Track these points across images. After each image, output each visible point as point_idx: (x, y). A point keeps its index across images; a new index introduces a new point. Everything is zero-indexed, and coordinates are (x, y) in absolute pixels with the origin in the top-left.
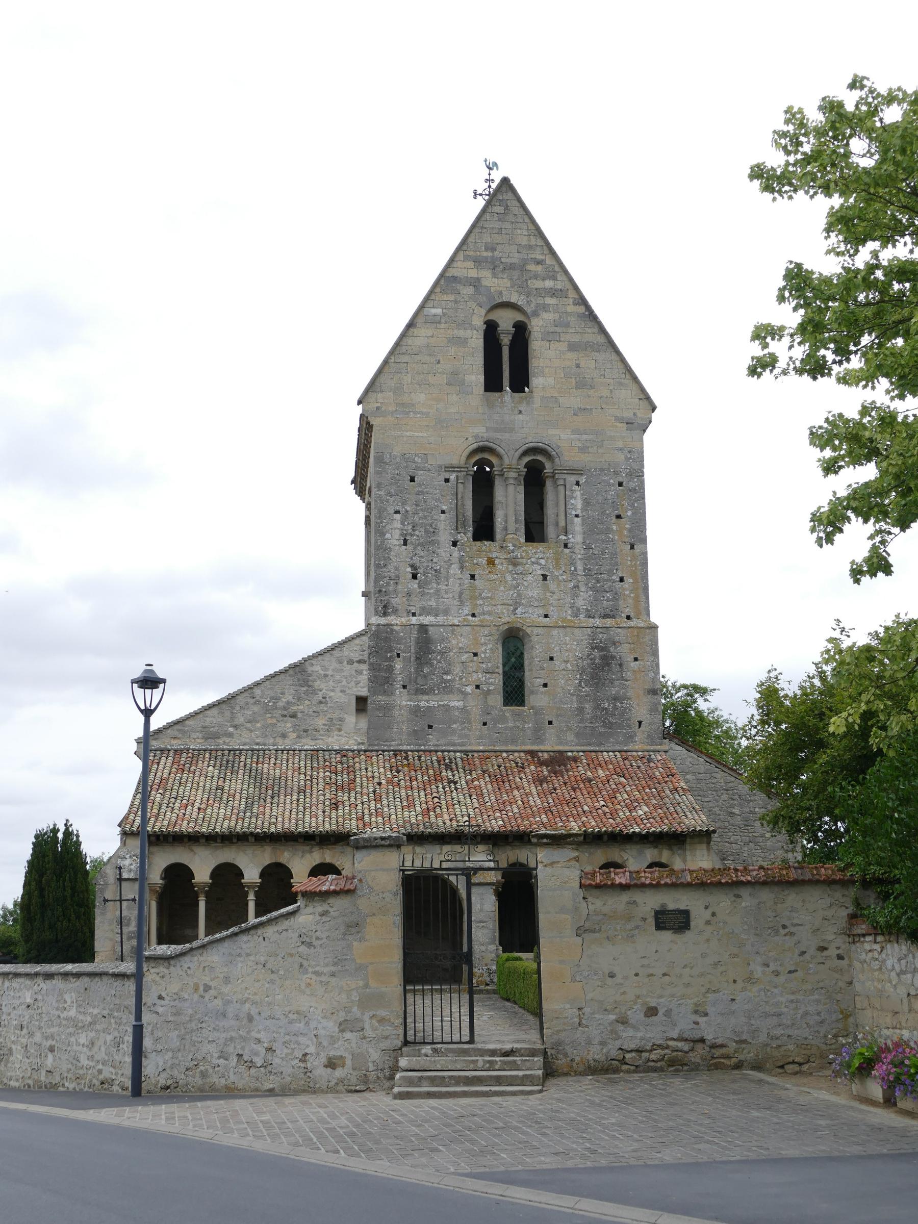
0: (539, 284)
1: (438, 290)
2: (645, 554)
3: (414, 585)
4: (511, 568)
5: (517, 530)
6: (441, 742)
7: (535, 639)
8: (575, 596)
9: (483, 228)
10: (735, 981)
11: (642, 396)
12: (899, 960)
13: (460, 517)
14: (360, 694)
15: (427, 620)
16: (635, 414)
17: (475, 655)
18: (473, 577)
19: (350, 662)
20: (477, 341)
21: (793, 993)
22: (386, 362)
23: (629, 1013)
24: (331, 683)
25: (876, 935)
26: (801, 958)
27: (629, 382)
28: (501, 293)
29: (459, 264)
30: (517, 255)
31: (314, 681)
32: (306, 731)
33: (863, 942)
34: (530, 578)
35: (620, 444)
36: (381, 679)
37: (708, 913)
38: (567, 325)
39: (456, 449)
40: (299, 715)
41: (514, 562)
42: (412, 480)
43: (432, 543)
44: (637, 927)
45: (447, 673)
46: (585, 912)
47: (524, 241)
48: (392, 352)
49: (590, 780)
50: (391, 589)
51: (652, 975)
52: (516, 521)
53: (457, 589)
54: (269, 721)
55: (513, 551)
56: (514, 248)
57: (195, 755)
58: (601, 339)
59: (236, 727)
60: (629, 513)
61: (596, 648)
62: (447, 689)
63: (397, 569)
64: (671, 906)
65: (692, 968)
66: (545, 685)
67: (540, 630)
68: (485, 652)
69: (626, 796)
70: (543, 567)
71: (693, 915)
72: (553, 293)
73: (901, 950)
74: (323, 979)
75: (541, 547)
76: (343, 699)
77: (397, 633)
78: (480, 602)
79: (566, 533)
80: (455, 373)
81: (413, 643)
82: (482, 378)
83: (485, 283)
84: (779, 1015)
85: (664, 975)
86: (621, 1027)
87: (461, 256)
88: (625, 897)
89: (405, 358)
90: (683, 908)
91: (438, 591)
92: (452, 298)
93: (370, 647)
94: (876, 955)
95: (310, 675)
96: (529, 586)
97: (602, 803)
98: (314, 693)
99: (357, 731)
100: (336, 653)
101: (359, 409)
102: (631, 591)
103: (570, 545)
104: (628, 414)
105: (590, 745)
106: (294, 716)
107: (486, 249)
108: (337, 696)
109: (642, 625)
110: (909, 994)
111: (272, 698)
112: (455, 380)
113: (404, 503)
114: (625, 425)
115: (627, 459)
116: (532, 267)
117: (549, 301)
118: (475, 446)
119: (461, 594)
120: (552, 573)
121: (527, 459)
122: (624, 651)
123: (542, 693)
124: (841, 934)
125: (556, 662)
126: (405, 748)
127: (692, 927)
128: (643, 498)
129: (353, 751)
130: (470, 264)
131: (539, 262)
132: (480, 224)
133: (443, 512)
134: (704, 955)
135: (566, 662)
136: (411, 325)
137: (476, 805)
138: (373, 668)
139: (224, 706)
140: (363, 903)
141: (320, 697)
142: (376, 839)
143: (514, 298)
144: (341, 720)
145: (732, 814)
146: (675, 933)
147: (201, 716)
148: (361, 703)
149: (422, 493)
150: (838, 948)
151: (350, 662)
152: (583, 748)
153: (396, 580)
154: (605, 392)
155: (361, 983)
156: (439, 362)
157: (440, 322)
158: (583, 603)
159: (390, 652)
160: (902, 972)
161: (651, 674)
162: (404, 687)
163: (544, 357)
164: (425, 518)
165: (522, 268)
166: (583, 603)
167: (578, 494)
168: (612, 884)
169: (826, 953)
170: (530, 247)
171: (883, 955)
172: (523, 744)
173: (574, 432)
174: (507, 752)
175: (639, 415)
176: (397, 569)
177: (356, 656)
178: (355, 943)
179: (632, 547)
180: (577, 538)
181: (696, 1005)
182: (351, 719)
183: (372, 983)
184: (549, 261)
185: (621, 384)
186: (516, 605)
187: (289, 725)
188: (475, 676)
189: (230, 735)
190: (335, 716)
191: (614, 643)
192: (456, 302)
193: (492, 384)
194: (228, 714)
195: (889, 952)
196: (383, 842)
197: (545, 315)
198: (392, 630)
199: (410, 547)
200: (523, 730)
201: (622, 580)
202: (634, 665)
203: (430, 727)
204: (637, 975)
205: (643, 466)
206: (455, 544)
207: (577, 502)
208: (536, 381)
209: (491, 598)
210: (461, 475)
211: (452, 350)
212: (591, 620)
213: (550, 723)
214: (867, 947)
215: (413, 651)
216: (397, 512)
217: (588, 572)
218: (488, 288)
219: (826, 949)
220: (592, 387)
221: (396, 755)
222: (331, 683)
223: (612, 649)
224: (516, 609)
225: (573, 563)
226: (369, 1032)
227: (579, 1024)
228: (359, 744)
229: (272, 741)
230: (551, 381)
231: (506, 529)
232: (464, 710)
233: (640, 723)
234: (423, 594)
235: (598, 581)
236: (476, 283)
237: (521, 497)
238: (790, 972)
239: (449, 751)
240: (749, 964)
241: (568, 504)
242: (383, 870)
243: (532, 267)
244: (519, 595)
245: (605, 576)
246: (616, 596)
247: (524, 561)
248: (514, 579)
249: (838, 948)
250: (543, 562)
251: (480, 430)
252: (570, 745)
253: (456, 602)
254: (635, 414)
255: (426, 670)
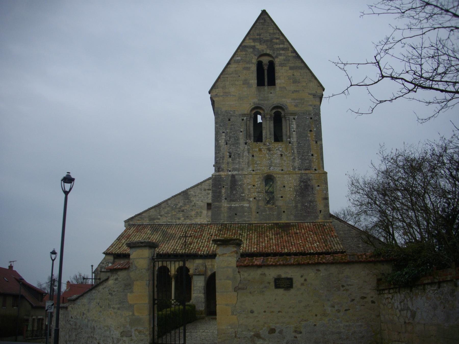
0: (277, 46)
1: (239, 51)
2: (321, 145)
3: (230, 160)
4: (268, 152)
5: (270, 138)
6: (240, 220)
7: (277, 179)
8: (294, 162)
9: (256, 28)
10: (316, 315)
11: (319, 85)
12: (400, 303)
13: (248, 133)
14: (208, 202)
15: (235, 173)
16: (316, 92)
17: (254, 186)
18: (253, 156)
19: (205, 190)
20: (254, 68)
21: (347, 322)
22: (219, 77)
23: (260, 331)
24: (197, 198)
25: (390, 289)
26: (352, 303)
27: (313, 80)
28: (263, 50)
29: (247, 41)
30: (269, 37)
31: (191, 197)
32: (187, 217)
33: (384, 294)
34: (275, 155)
35: (311, 103)
36: (217, 196)
37: (302, 280)
38: (289, 60)
39: (246, 108)
40: (185, 211)
41: (269, 150)
42: (229, 120)
43: (237, 143)
44: (265, 287)
45: (242, 193)
46: (239, 279)
47: (271, 31)
48: (222, 74)
49: (297, 233)
50: (221, 161)
51: (273, 312)
52: (270, 134)
53: (247, 161)
54: (174, 213)
55: (269, 145)
56: (268, 34)
57: (145, 226)
58: (303, 65)
59: (161, 216)
60: (315, 129)
61: (302, 182)
62: (243, 199)
63: (223, 154)
64: (283, 276)
65: (293, 308)
66: (282, 197)
67: (279, 176)
68: (258, 185)
69: (311, 239)
70: (281, 151)
71: (294, 280)
72: (283, 49)
73: (401, 297)
74: (115, 311)
75: (280, 144)
76: (202, 204)
77: (223, 178)
78: (256, 165)
79: (290, 138)
80: (246, 80)
81: (229, 182)
82: (256, 81)
83: (257, 47)
84: (339, 333)
85: (279, 312)
86: (256, 339)
87: (248, 38)
88: (260, 271)
89: (227, 76)
90: (289, 277)
91: (239, 162)
92: (244, 53)
93: (212, 184)
94: (390, 300)
95: (189, 195)
96: (277, 159)
97: (300, 242)
98: (191, 202)
99: (207, 216)
100: (199, 187)
101: (209, 96)
102: (316, 159)
103: (291, 142)
104: (314, 92)
105: (300, 220)
106: (183, 211)
107: (257, 35)
108: (200, 203)
109: (321, 172)
110: (405, 322)
111: (175, 204)
112: (246, 83)
113: (226, 129)
114: (312, 96)
115: (313, 109)
116: (275, 41)
117: (281, 52)
118: (253, 106)
119: (248, 163)
120: (284, 153)
121: (274, 111)
122: (314, 183)
123: (280, 200)
124: (374, 289)
125: (286, 188)
126: (226, 223)
127: (294, 287)
128: (320, 123)
129: (205, 224)
130: (251, 41)
131: (277, 39)
132: (255, 26)
133: (241, 132)
134: (300, 302)
135: (290, 188)
136: (229, 64)
137: (248, 243)
138: (214, 192)
139: (157, 208)
140: (132, 274)
141: (193, 204)
142: (138, 243)
143: (268, 52)
144: (201, 212)
145: (359, 247)
146: (285, 290)
147: (148, 212)
148: (209, 205)
149: (233, 125)
150: (372, 297)
151: (205, 190)
152: (297, 222)
153: (223, 158)
154: (304, 84)
155: (131, 313)
156: (239, 76)
157: (240, 62)
158: (297, 164)
159: (221, 186)
160: (402, 310)
161: (325, 192)
162: (226, 199)
163: (282, 75)
164: (234, 134)
165: (271, 41)
166: (297, 164)
167: (294, 123)
168: (252, 265)
169: (365, 300)
170: (274, 34)
171: (393, 300)
172: (273, 220)
173: (292, 99)
174: (266, 223)
175: (318, 92)
176: (223, 154)
177: (207, 187)
178: (129, 294)
179: (316, 142)
180: (294, 139)
181: (296, 328)
182: (205, 212)
183: (136, 314)
184: (281, 38)
185: (310, 81)
186: (270, 166)
187: (181, 215)
188: (254, 194)
189: (159, 219)
190: (199, 211)
191: (309, 180)
192: (246, 54)
193: (260, 83)
194: (158, 211)
195: (396, 298)
196: (141, 245)
197: (280, 57)
198: (221, 177)
199: (228, 146)
200: (273, 215)
201: (312, 155)
202: (317, 188)
203: (236, 214)
204: (265, 312)
205: (320, 111)
206: (246, 143)
207: (294, 126)
208: (277, 81)
209: (260, 164)
210: (248, 117)
211: (245, 72)
212: (300, 171)
213: (284, 212)
214: (386, 296)
215: (229, 184)
216: (223, 132)
217: (299, 152)
218: (258, 49)
219: (365, 298)
220: (299, 82)
221: (222, 225)
222: (197, 198)
223: (309, 182)
224: (270, 168)
225: (293, 149)
226: (134, 338)
227: (235, 336)
228: (208, 221)
229: (174, 221)
230: (283, 81)
231: (266, 137)
232: (249, 207)
233: (320, 211)
234: (234, 163)
235: (303, 156)
236: (253, 47)
237: (272, 125)
238: (346, 310)
239: (243, 224)
240: (324, 306)
241: (291, 127)
242: (142, 258)
243: (275, 41)
244: (271, 162)
245: (306, 154)
246: (311, 161)
247: (273, 149)
248: (269, 156)
249: (372, 297)
250: (281, 149)
251: (256, 100)
252: (292, 220)
253: (246, 166)
254: (316, 92)
255: (234, 192)
